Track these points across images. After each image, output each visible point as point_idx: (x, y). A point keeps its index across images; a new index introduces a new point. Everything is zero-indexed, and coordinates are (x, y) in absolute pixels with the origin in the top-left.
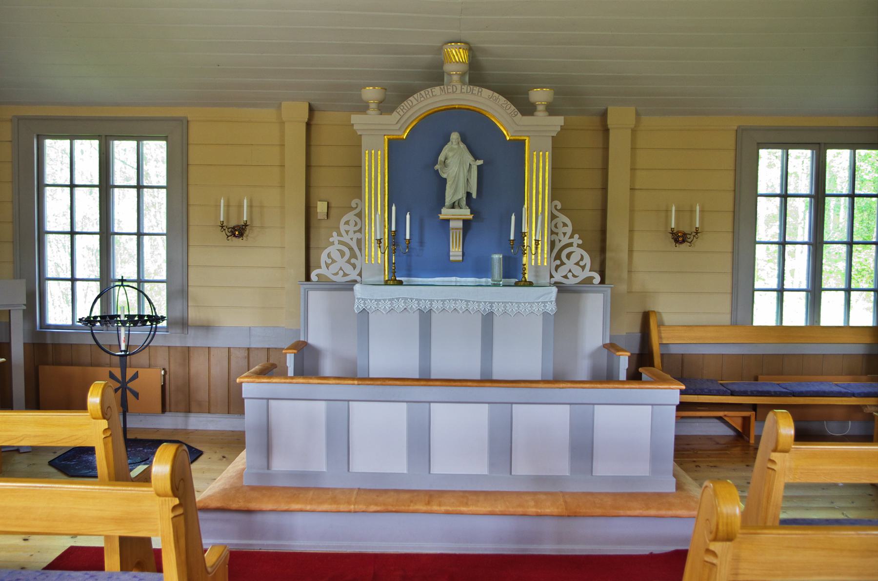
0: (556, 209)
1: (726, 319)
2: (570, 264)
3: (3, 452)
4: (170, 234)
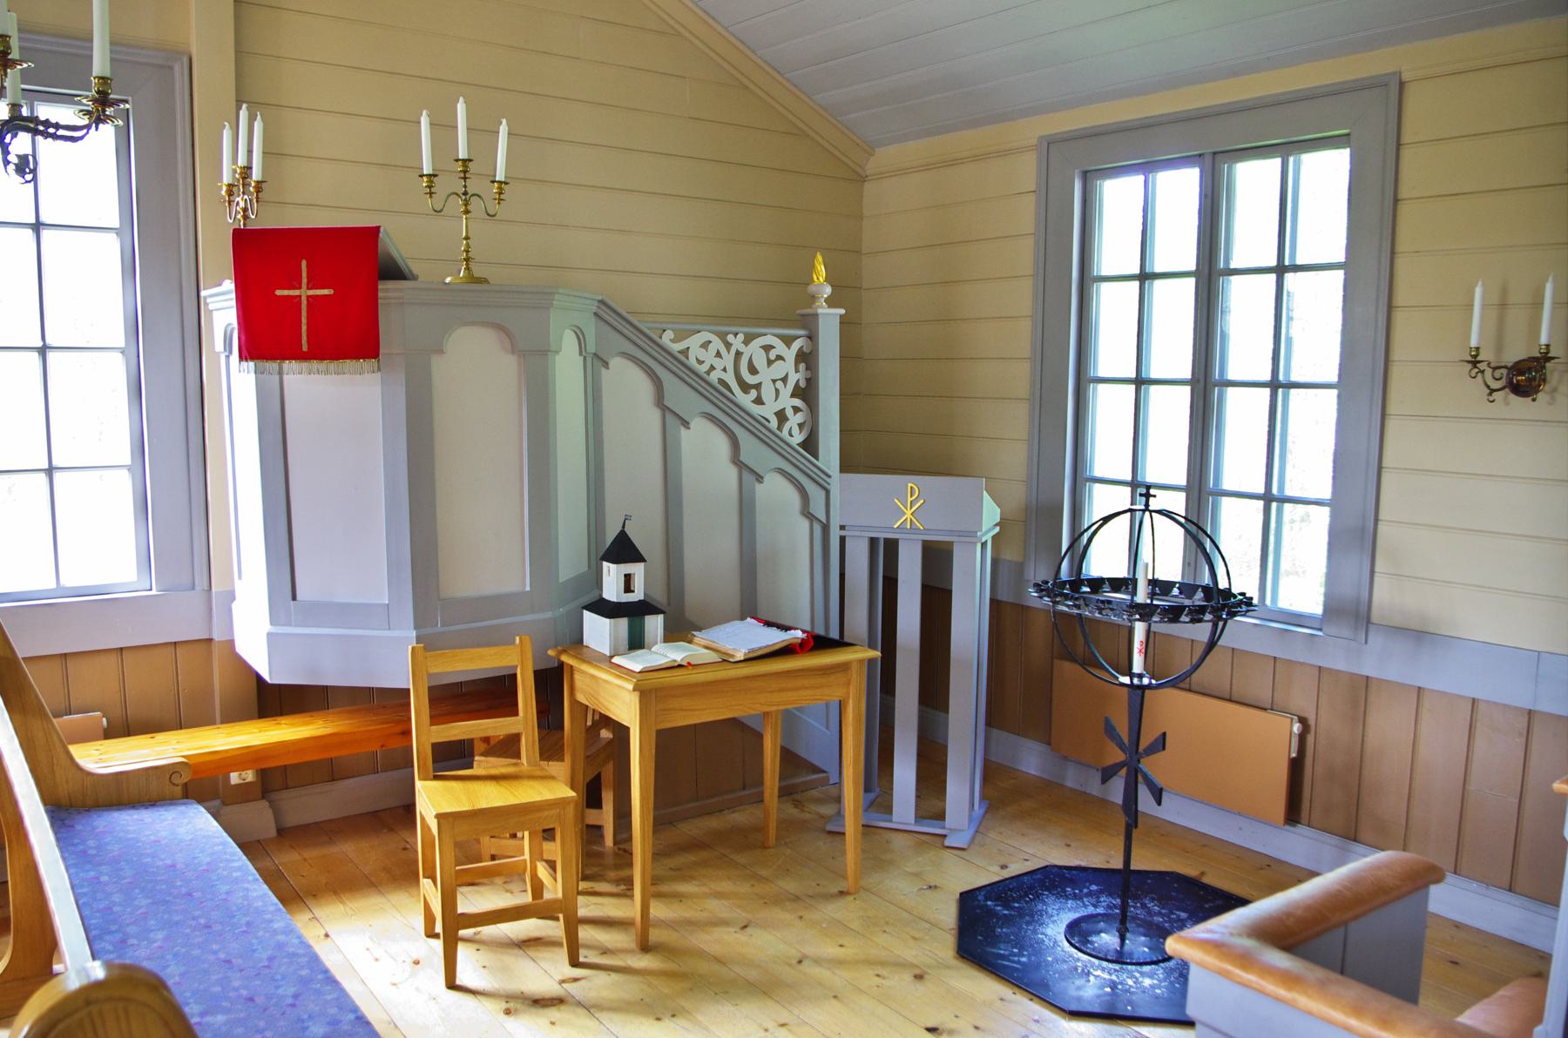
4: (1345, 384)
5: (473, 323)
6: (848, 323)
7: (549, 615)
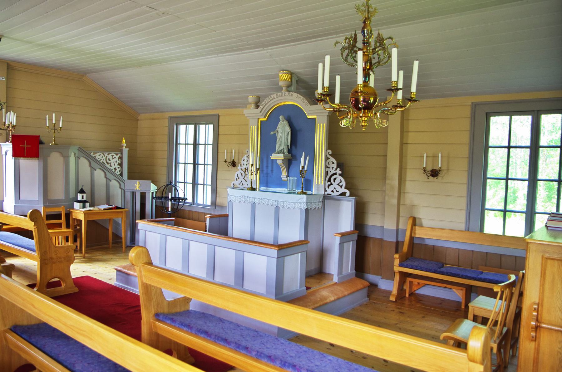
0: (329, 155)
1: (462, 226)
2: (335, 184)
3: (59, 237)
4: (213, 165)
5: (55, 151)
6: (162, 143)
7: (68, 203)
